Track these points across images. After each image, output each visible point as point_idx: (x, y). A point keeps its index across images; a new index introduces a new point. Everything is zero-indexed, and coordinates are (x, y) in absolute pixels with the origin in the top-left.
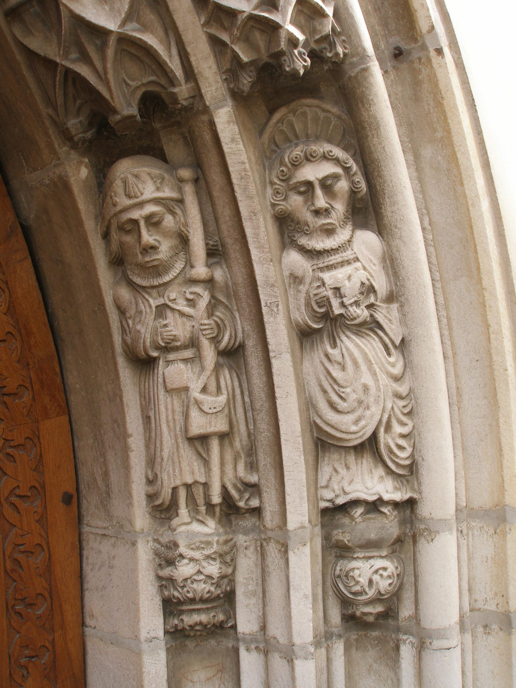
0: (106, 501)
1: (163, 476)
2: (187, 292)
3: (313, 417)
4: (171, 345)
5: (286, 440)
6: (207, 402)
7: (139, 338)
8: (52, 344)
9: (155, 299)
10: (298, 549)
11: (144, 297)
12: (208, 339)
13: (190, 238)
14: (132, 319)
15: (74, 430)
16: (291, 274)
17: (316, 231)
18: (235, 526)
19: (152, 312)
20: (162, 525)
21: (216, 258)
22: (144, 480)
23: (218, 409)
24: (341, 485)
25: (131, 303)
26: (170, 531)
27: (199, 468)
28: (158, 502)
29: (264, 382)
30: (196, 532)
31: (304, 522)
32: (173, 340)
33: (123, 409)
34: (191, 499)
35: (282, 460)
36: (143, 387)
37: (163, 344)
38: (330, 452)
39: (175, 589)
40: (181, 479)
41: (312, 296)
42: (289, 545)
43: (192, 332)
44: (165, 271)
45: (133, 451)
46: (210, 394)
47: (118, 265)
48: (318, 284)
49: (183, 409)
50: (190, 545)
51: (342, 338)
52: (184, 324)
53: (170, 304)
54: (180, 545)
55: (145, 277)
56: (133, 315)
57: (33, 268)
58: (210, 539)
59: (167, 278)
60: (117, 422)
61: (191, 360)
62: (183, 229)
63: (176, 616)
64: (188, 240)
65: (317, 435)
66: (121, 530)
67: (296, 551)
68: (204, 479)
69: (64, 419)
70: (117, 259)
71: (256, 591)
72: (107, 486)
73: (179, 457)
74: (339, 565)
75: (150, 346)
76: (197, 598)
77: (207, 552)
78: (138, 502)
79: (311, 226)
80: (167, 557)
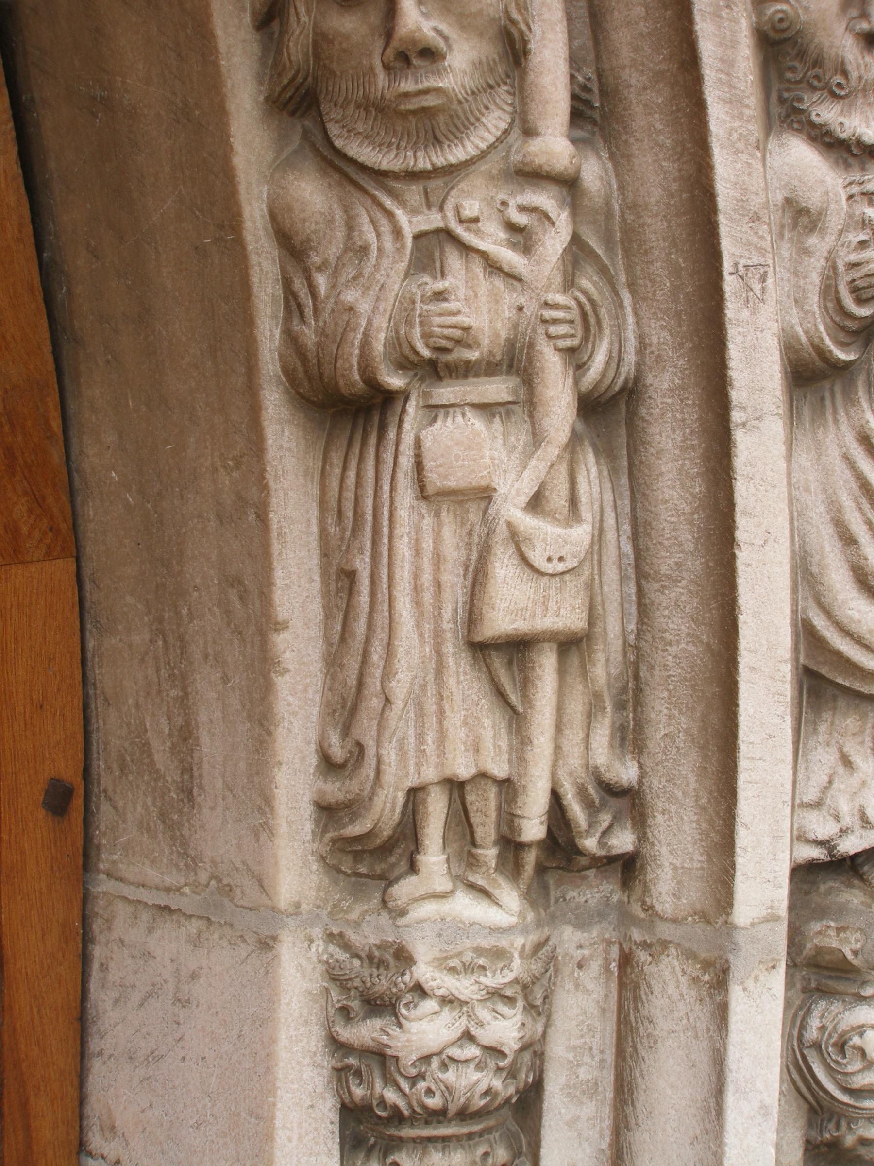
0: (180, 812)
1: (383, 752)
2: (512, 203)
3: (804, 610)
4: (450, 358)
5: (753, 669)
6: (544, 540)
7: (348, 328)
8: (47, 349)
9: (414, 212)
10: (756, 979)
11: (380, 206)
12: (560, 350)
13: (532, 46)
14: (329, 272)
15: (88, 605)
16: (788, 201)
17: (864, 90)
18: (557, 901)
19: (400, 250)
20: (357, 892)
21: (582, 129)
22: (313, 760)
23: (570, 564)
24: (858, 801)
25: (331, 222)
26: (385, 915)
27: (495, 735)
28: (355, 829)
29: (694, 496)
30: (459, 917)
31: (776, 904)
32: (458, 342)
33: (266, 547)
34: (461, 823)
35: (736, 726)
36: (334, 484)
37: (426, 353)
38: (834, 709)
39: (389, 1080)
40: (441, 765)
41: (841, 268)
42: (733, 967)
43: (516, 326)
44: (454, 130)
45: (287, 671)
46: (550, 515)
47: (292, 114)
48: (862, 237)
49: (468, 555)
50: (446, 958)
51: (838, 417)
52: (495, 298)
53: (459, 230)
54: (416, 956)
55: (390, 145)
56: (332, 260)
57: (11, 125)
58: (504, 943)
59: (457, 154)
60: (240, 582)
61: (502, 410)
62: (516, 16)
63: (375, 1154)
64: (526, 53)
65: (806, 662)
66: (226, 901)
67: (750, 983)
68: (506, 767)
69: (64, 568)
70: (298, 89)
71: (596, 1084)
72: (187, 770)
73: (442, 698)
74: (816, 1013)
75: (385, 354)
76: (453, 1109)
77: (492, 980)
78: (290, 823)
79: (854, 75)
80: (371, 987)
